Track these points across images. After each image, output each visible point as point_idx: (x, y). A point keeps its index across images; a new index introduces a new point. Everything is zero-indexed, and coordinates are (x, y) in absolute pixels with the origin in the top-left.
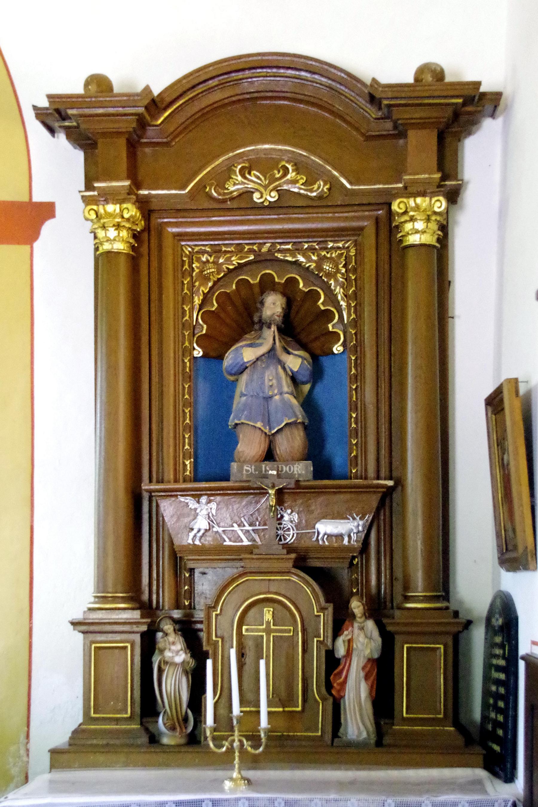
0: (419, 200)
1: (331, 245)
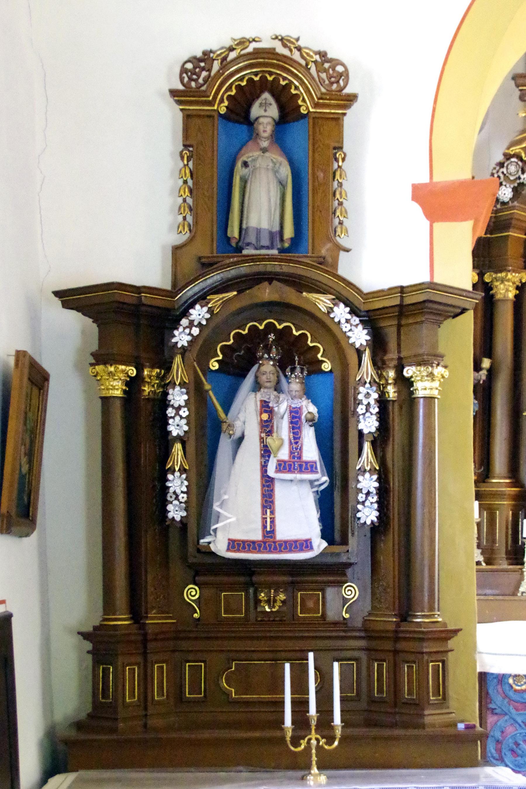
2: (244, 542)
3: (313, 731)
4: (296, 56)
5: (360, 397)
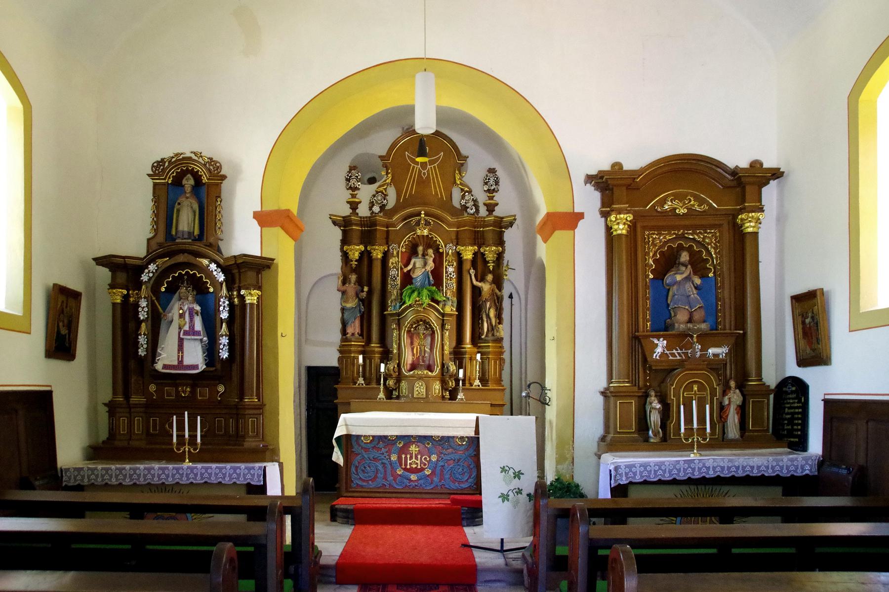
0: (753, 214)
1: (709, 231)
2: (170, 365)
3: (187, 445)
4: (200, 160)
5: (221, 303)
